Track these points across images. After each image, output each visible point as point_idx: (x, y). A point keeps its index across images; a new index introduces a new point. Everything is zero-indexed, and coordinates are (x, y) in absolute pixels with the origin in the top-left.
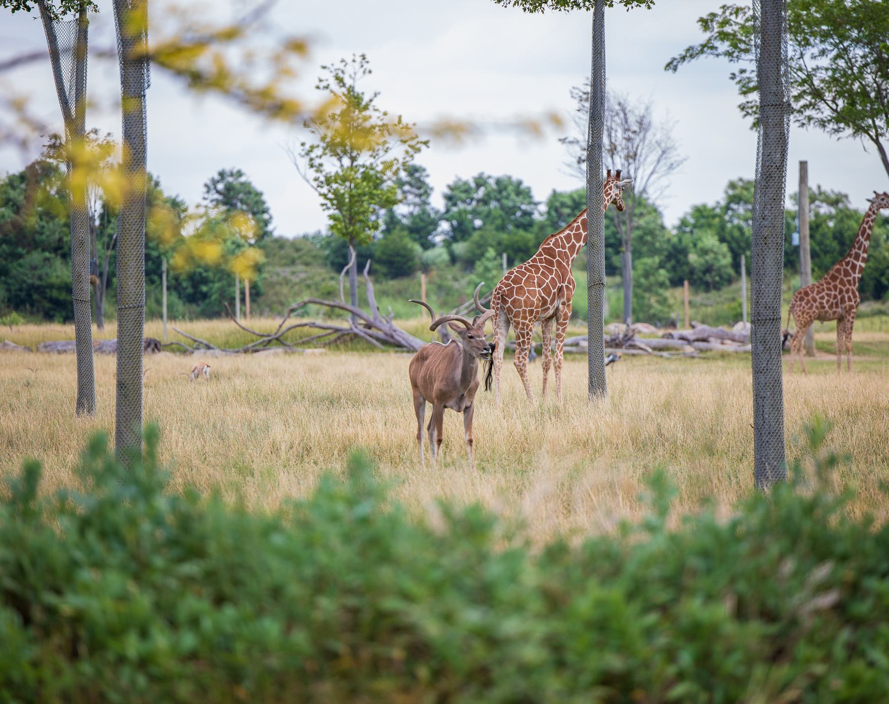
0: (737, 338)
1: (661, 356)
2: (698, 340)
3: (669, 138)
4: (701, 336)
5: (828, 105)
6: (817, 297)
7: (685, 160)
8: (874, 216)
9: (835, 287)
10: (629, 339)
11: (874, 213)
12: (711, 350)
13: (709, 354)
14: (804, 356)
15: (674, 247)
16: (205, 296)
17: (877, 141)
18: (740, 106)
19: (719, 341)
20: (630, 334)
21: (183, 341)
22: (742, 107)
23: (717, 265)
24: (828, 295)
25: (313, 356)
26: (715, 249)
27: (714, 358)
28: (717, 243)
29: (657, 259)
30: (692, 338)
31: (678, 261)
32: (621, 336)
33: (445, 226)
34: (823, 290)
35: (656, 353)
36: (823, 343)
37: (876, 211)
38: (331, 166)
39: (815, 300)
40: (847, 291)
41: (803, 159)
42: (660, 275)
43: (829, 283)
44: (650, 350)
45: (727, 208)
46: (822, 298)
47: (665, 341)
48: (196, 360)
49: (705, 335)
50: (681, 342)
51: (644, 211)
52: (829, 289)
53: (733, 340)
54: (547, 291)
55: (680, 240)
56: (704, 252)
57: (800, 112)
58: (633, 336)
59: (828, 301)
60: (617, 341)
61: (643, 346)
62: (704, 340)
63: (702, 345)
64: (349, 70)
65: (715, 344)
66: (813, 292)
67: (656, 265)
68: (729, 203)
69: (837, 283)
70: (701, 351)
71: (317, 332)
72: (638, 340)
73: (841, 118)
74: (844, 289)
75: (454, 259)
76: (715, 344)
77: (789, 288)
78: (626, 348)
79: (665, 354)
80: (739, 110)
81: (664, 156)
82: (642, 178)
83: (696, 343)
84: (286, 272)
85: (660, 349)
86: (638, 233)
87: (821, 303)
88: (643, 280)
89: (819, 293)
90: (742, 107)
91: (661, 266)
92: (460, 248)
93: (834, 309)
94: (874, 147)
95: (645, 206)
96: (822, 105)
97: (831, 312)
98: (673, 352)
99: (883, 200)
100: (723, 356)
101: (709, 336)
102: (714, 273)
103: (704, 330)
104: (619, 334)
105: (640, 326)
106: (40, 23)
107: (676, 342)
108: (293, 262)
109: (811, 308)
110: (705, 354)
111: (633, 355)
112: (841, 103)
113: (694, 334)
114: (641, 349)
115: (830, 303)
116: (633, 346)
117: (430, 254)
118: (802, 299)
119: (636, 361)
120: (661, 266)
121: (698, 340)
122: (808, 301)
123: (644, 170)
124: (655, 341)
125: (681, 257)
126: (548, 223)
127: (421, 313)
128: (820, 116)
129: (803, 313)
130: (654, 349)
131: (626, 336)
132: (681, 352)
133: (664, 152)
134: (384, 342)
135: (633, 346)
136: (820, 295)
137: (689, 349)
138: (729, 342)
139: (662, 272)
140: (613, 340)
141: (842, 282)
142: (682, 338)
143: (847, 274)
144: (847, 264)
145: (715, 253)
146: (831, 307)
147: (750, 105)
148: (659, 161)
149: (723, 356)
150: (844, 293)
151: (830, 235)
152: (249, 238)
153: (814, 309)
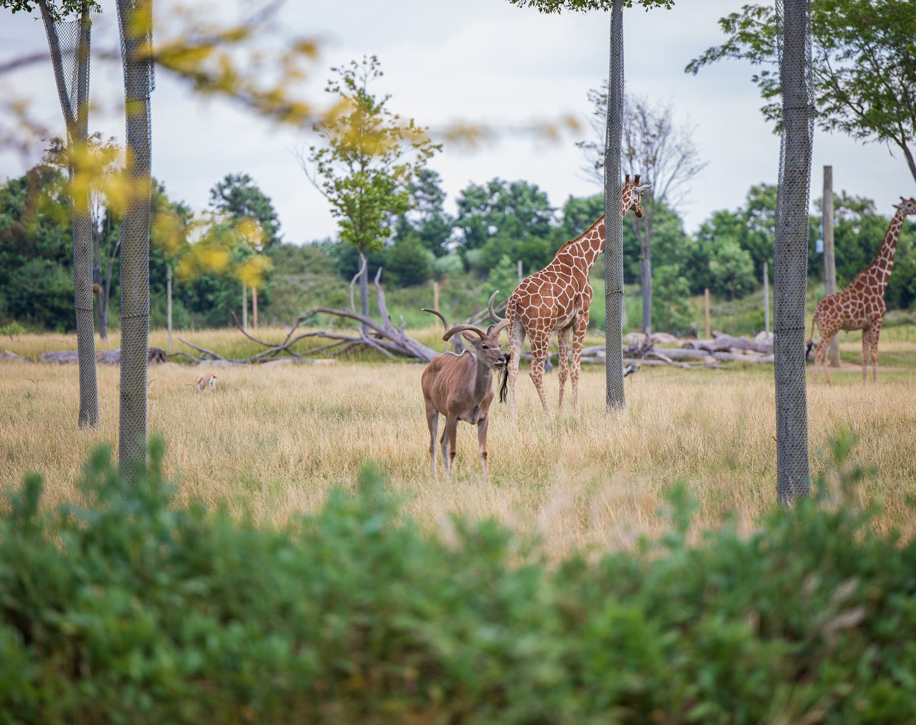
0: (759, 348)
1: (681, 367)
2: (719, 350)
3: (689, 142)
4: (722, 346)
5: (853, 108)
6: (842, 306)
7: (706, 164)
8: (900, 223)
9: (861, 296)
10: (648, 349)
11: (900, 219)
12: (732, 360)
13: (730, 365)
14: (829, 366)
15: (695, 254)
16: (211, 305)
17: (903, 146)
18: (762, 110)
19: (741, 351)
20: (650, 344)
21: (188, 351)
22: (765, 111)
23: (738, 273)
24: (853, 304)
25: (323, 366)
26: (737, 257)
27: (736, 369)
28: (739, 250)
29: (677, 267)
30: (713, 348)
31: (699, 269)
32: (640, 346)
33: (458, 233)
34: (848, 299)
35: (676, 363)
36: (848, 353)
37: (902, 218)
38: (342, 171)
39: (839, 309)
40: (873, 300)
41: (828, 164)
42: (680, 283)
43: (854, 292)
44: (670, 361)
45: (749, 214)
46: (847, 307)
47: (685, 351)
48: (202, 371)
49: (727, 345)
50: (702, 352)
51: (664, 217)
52: (854, 298)
53: (756, 350)
54: (563, 299)
55: (701, 247)
56: (726, 259)
57: (824, 115)
58: (652, 346)
59: (853, 310)
60: (636, 352)
61: (662, 356)
62: (726, 350)
63: (723, 355)
64: (360, 72)
65: (737, 354)
66: (837, 301)
67: (676, 273)
68: (751, 209)
69: (863, 291)
70: (723, 361)
71: (326, 342)
72: (658, 350)
73: (866, 121)
74: (870, 298)
75: (467, 267)
76: (737, 354)
77: (813, 297)
78: (645, 359)
79: (685, 364)
80: (761, 113)
81: (684, 161)
82: (661, 184)
83: (717, 354)
84: (295, 280)
85: (681, 360)
86: (657, 240)
87: (846, 312)
88: (662, 289)
89: (843, 301)
90: (765, 111)
91: (681, 274)
92: (474, 255)
93: (860, 319)
94: (901, 151)
95: (665, 212)
96: (847, 108)
97: (856, 321)
98: (694, 363)
99: (910, 206)
100: (745, 366)
101: (731, 346)
102: (735, 282)
103: (725, 340)
104: (638, 344)
105: (659, 336)
106: (41, 24)
107: (696, 352)
108: (302, 270)
109: (835, 317)
110: (726, 365)
111: (653, 366)
112: (866, 106)
113: (716, 344)
114: (660, 359)
115: (855, 312)
116: (652, 357)
117: (443, 262)
118: (826, 308)
119: (655, 372)
120: (681, 274)
121: (719, 350)
122: (833, 310)
123: (664, 175)
124: (675, 352)
125: (702, 265)
126: (564, 229)
127: (434, 322)
128: (844, 119)
129: (827, 323)
130: (674, 359)
131: (645, 346)
132: (702, 362)
133: (684, 157)
134: (396, 352)
135: (652, 357)
136: (845, 304)
137: (710, 360)
138: (751, 352)
139: (682, 280)
140: (632, 350)
141: (867, 291)
142: (703, 348)
143: (872, 282)
144: (873, 271)
145: (737, 261)
146: (856, 316)
147: (772, 108)
148: (679, 166)
149: (745, 366)
150: (870, 302)
151: (855, 242)
152: (257, 245)
153: (839, 318)
